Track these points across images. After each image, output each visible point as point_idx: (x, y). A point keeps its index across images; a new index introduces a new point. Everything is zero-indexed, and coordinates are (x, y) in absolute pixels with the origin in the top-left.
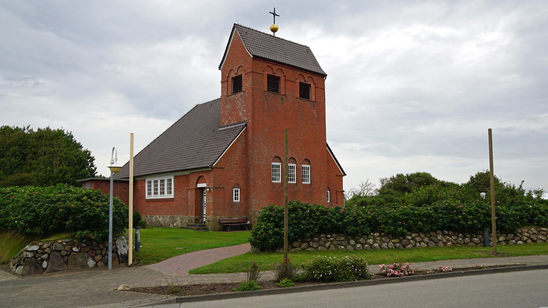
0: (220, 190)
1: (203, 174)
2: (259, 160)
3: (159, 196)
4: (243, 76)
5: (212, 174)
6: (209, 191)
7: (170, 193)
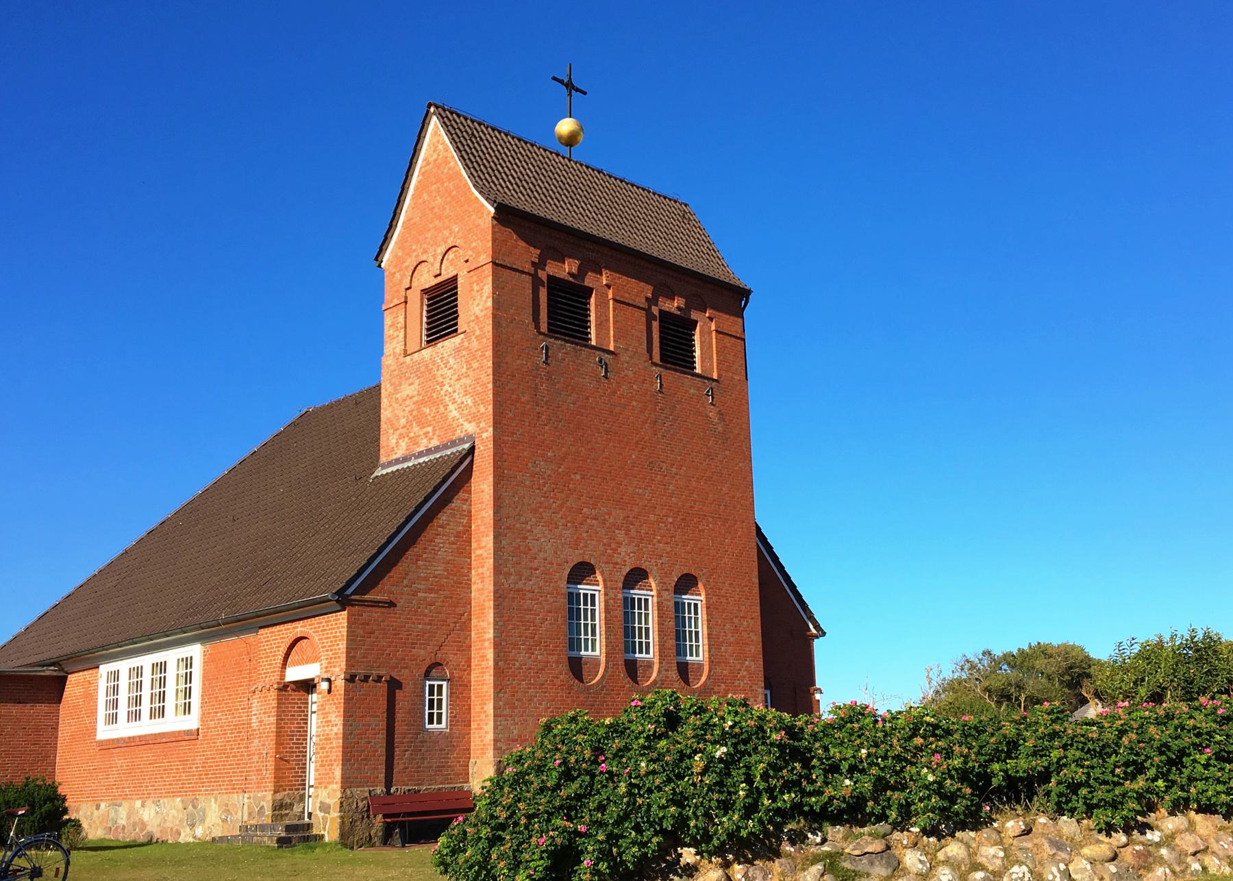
2: (520, 575)
3: (147, 726)
4: (460, 281)
7: (187, 709)
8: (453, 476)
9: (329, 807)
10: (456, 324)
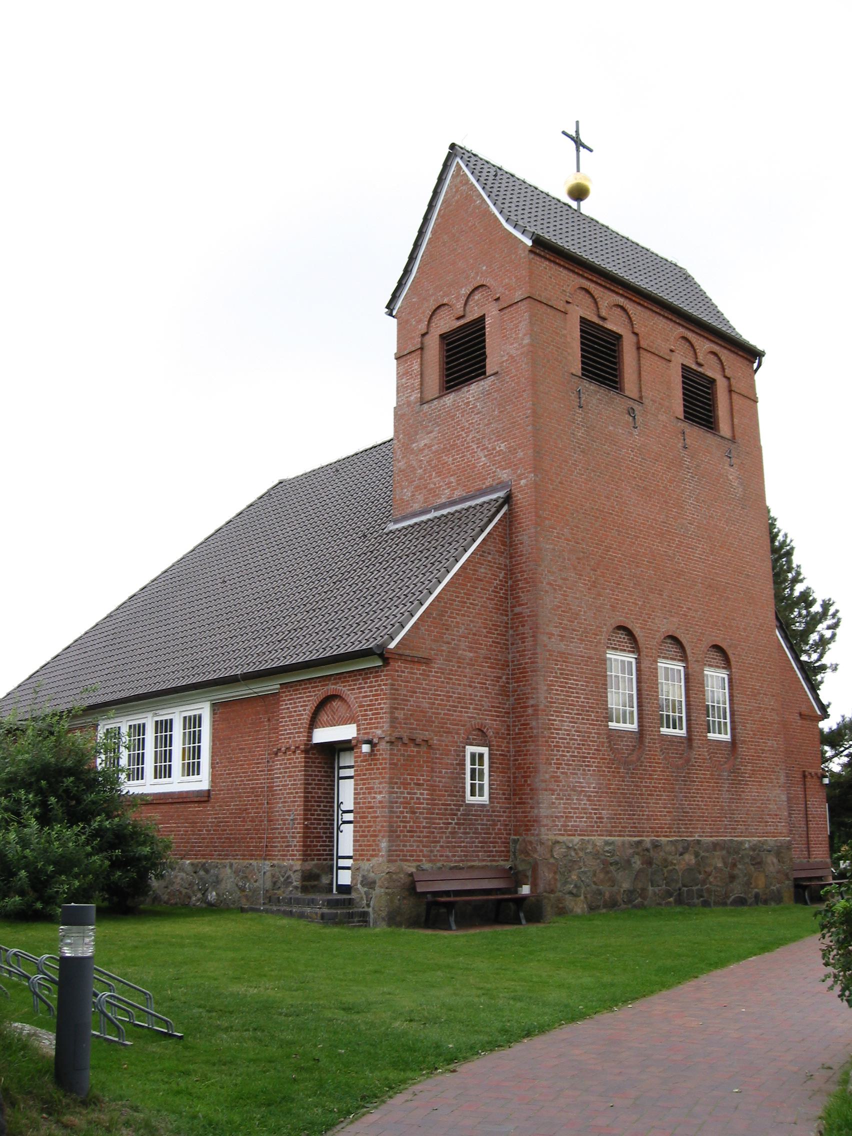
0: (412, 748)
1: (340, 688)
4: (488, 321)
5: (382, 684)
6: (372, 753)
10: (484, 366)
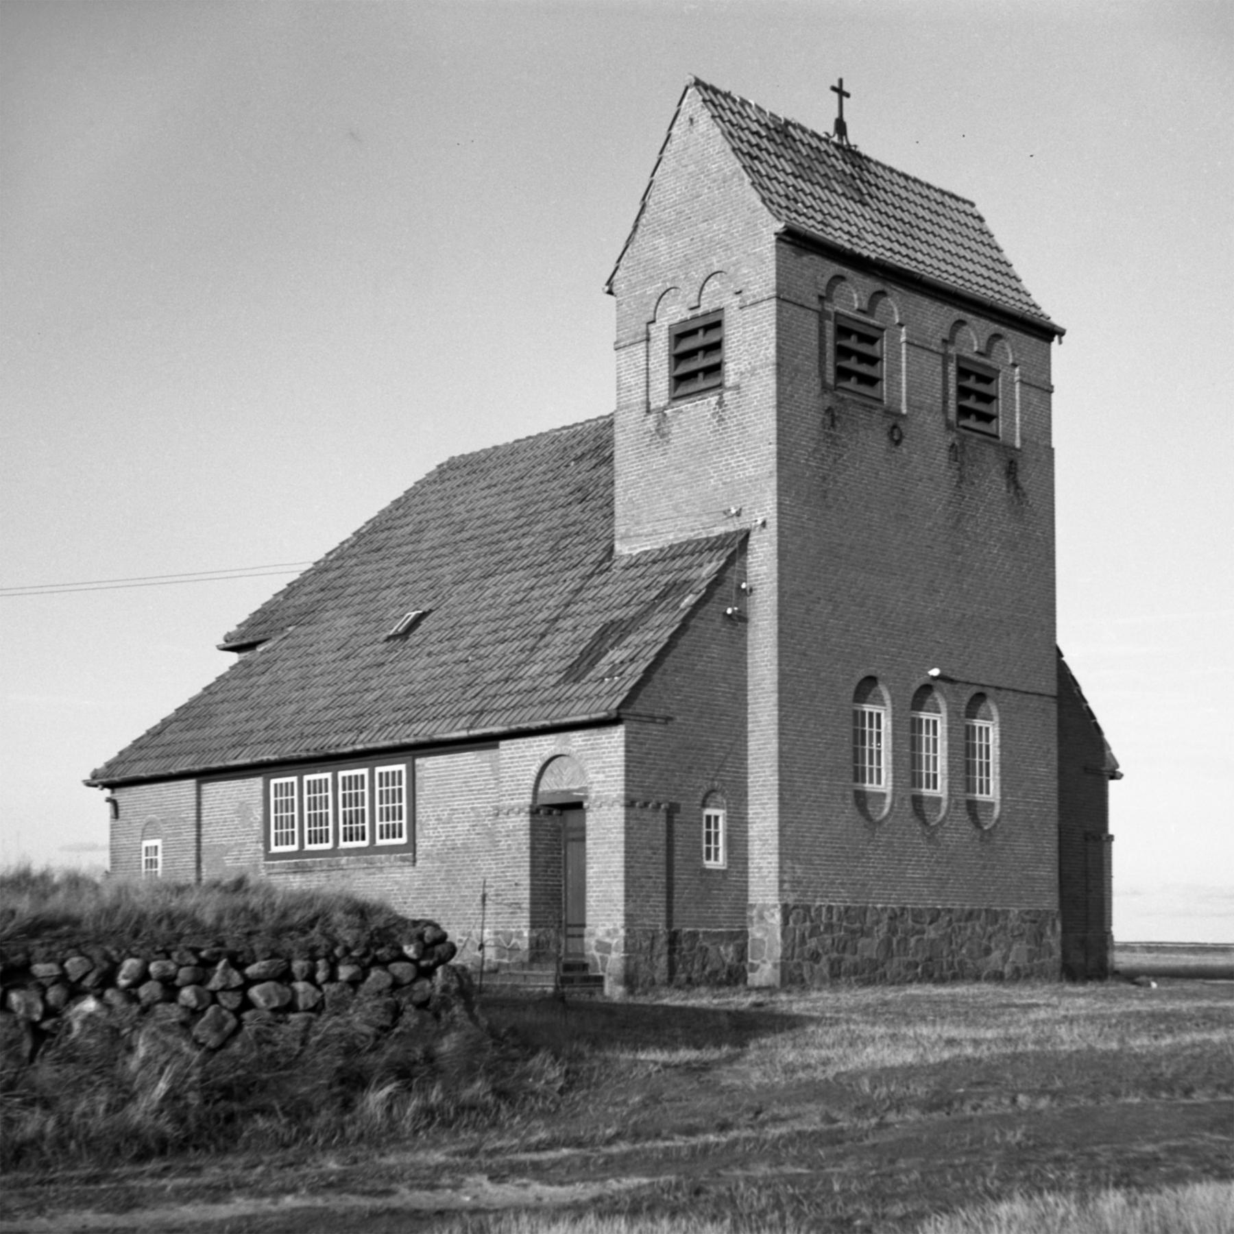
8: (810, 937)
9: (609, 946)
